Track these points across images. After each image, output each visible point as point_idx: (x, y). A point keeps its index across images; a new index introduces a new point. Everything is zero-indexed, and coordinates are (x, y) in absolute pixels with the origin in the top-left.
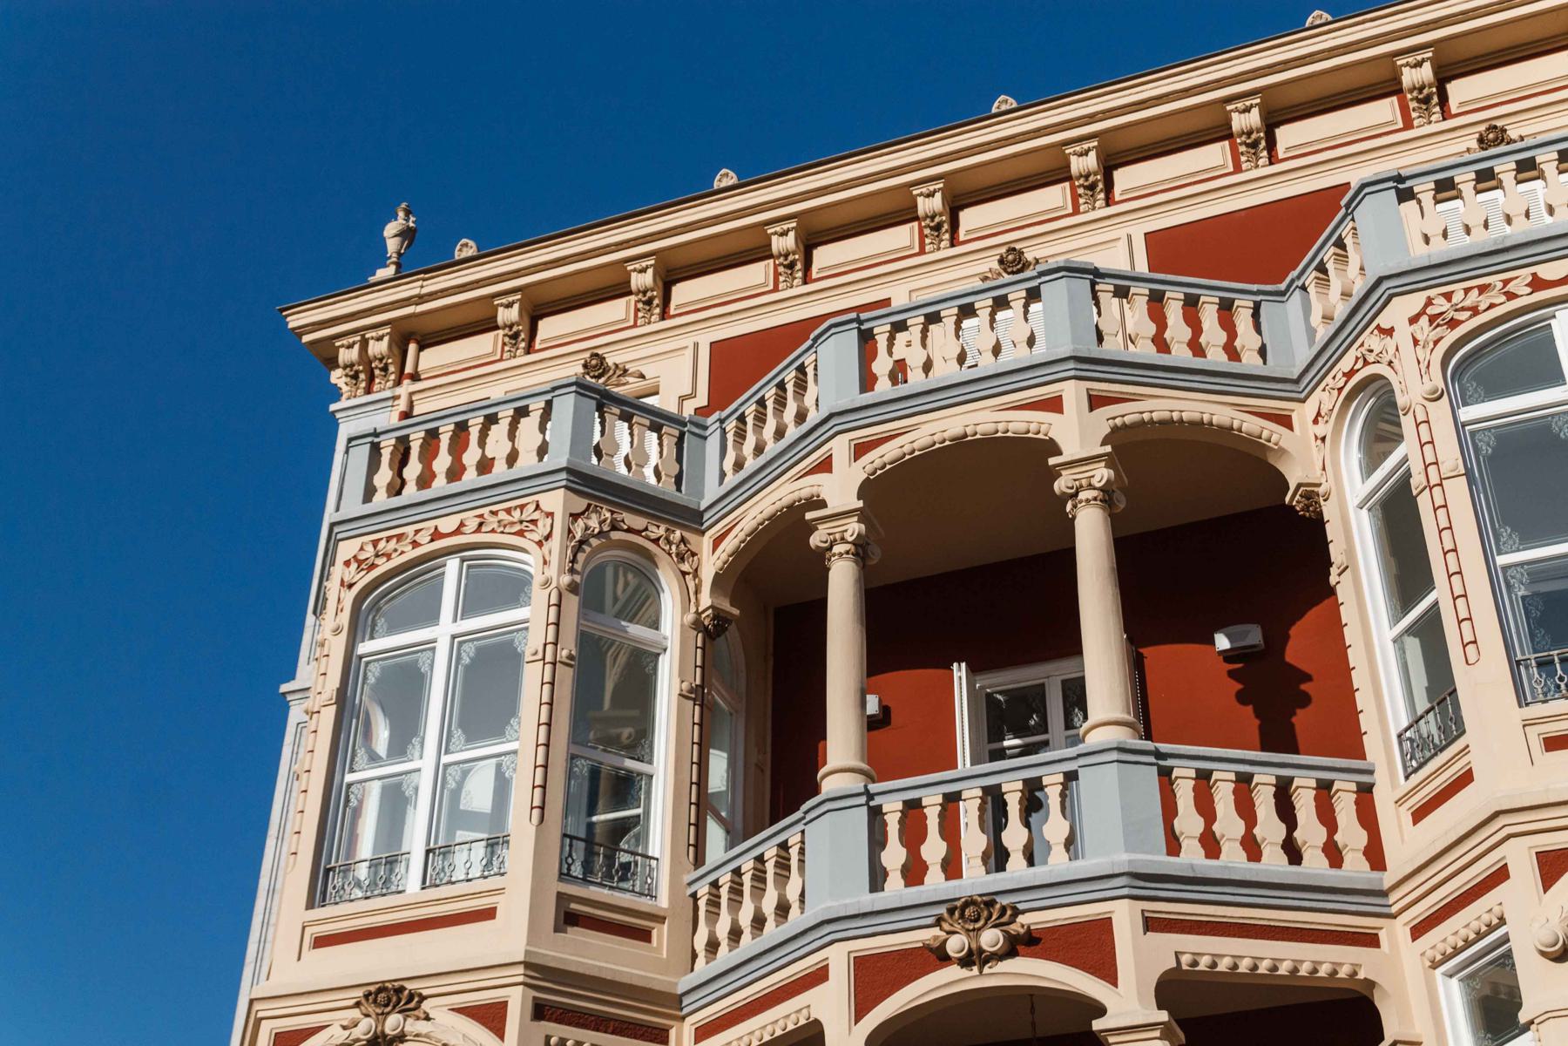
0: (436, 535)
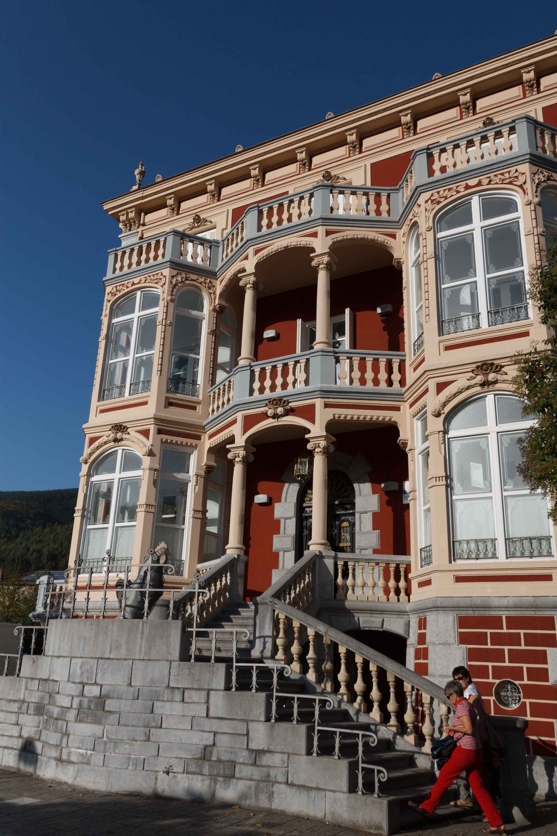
0: (133, 284)
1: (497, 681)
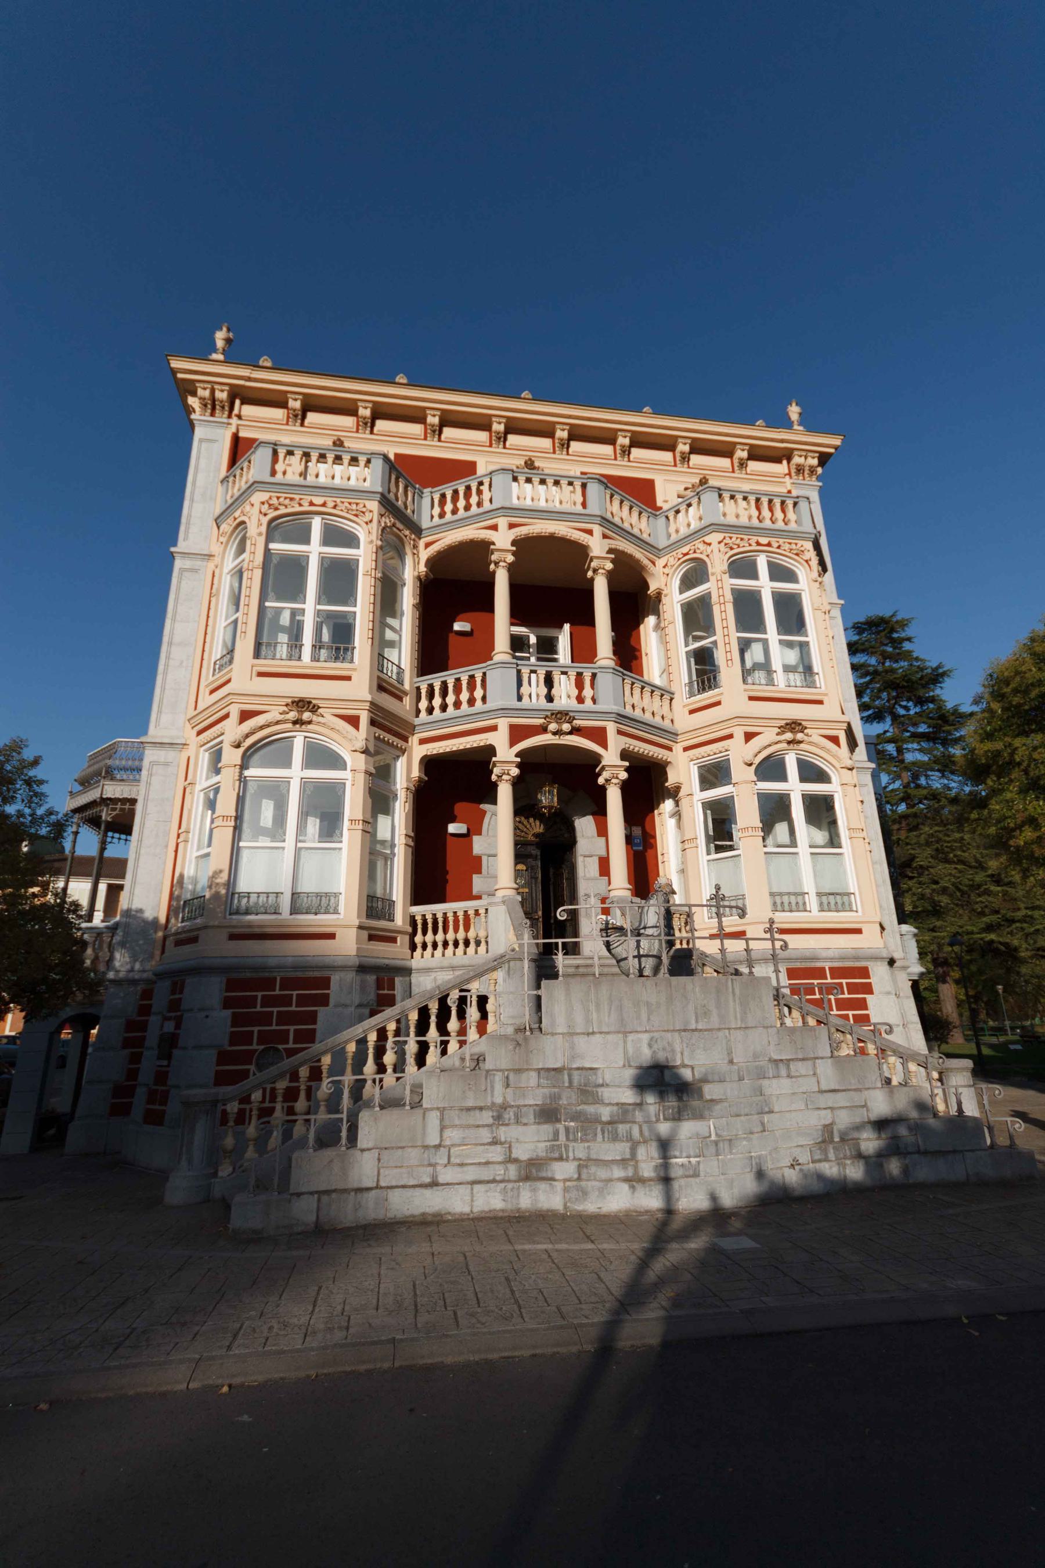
0: (311, 504)
1: (262, 1047)
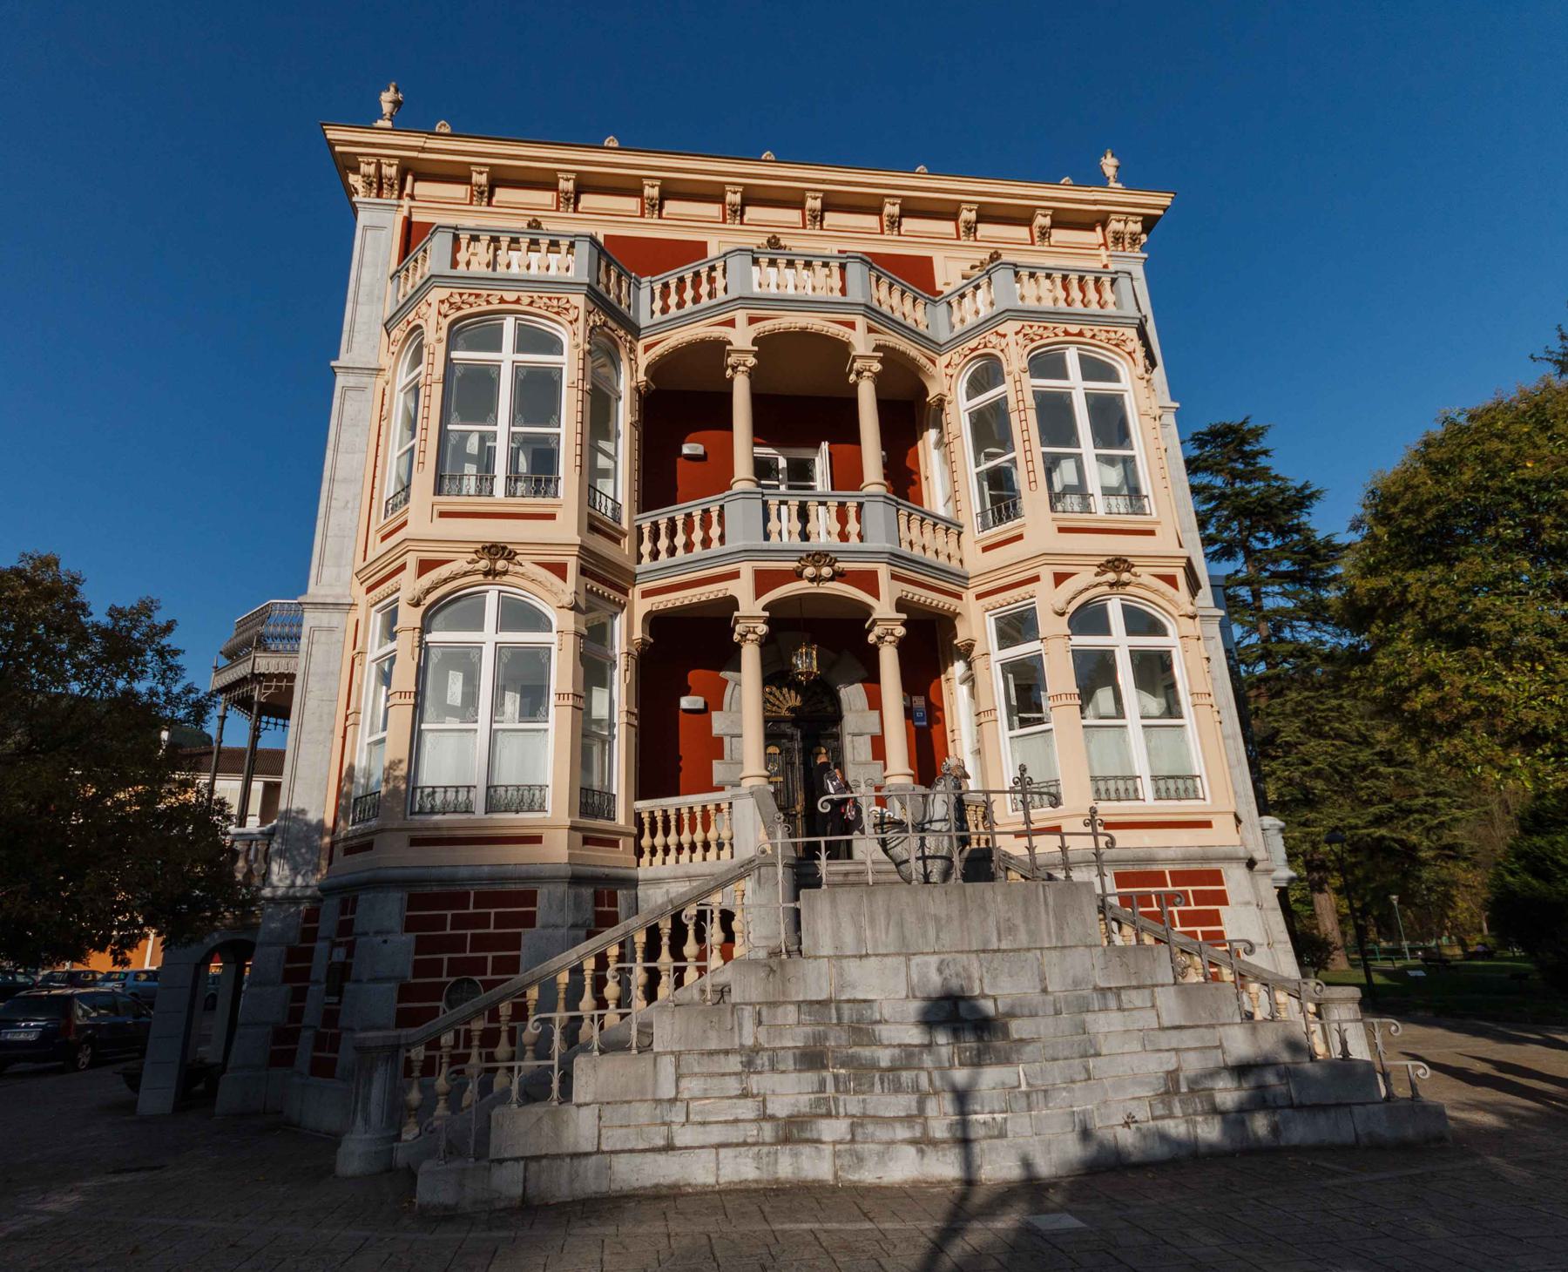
0: (502, 301)
1: (453, 979)
